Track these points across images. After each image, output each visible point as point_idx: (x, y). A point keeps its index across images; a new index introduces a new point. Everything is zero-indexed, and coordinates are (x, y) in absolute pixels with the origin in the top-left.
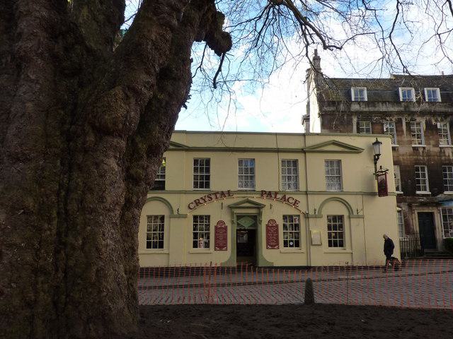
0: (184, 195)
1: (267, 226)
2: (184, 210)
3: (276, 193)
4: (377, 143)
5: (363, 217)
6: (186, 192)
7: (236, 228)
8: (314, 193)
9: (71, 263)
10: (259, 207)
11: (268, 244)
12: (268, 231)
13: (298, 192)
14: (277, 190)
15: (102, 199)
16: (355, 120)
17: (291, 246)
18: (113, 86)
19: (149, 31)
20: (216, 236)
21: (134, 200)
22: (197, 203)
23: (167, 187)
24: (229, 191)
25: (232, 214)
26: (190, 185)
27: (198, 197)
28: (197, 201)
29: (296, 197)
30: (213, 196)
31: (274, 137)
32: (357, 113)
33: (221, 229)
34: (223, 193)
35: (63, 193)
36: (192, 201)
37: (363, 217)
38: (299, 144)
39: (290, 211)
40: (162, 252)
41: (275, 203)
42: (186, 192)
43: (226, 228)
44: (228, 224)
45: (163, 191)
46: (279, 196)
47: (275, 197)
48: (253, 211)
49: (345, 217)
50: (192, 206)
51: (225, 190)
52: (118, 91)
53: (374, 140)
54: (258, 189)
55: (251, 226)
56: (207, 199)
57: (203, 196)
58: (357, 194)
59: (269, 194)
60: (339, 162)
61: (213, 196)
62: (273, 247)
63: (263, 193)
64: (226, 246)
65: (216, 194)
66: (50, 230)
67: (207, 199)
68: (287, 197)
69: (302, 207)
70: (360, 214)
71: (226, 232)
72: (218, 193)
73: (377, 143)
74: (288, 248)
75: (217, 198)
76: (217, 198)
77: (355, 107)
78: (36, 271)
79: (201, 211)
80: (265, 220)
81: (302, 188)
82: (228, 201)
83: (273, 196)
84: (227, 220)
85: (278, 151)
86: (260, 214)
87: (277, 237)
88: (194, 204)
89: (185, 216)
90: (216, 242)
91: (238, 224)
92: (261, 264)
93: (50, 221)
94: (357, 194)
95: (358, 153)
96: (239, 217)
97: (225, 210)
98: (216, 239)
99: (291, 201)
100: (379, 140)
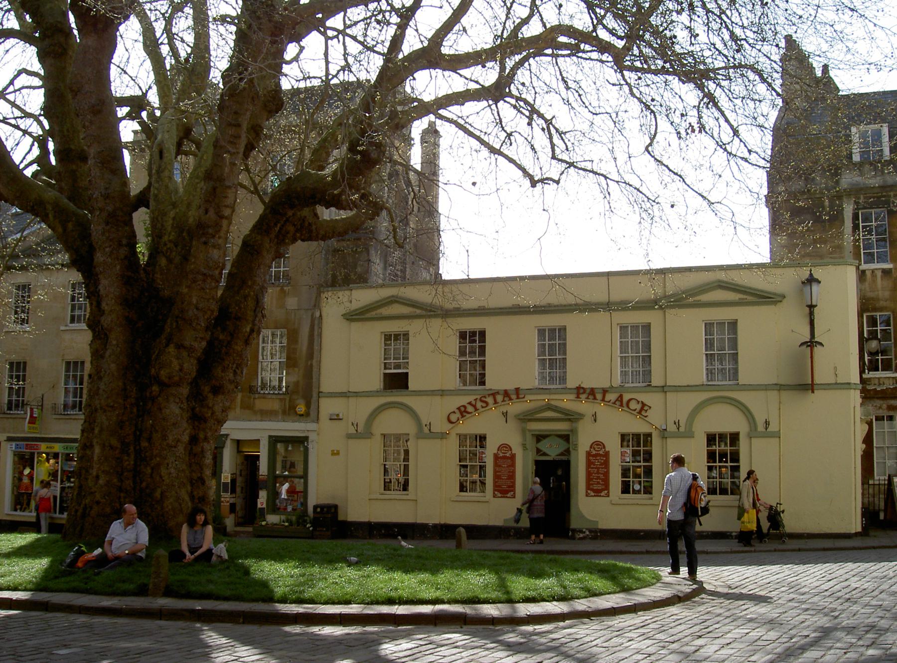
0: (437, 399)
1: (588, 454)
2: (440, 426)
3: (605, 391)
4: (811, 280)
5: (777, 435)
6: (442, 393)
7: (532, 456)
8: (678, 389)
9: (144, 485)
10: (572, 417)
11: (588, 487)
12: (589, 464)
13: (649, 387)
14: (606, 385)
15: (164, 437)
16: (848, 210)
17: (635, 492)
18: (167, 345)
19: (190, 297)
20: (495, 472)
21: (202, 435)
22: (463, 411)
23: (412, 385)
24: (517, 389)
25: (524, 431)
26: (452, 380)
27: (463, 400)
28: (463, 409)
29: (642, 397)
30: (490, 400)
31: (605, 279)
32: (855, 191)
33: (505, 459)
34: (506, 393)
35: (138, 433)
36: (454, 408)
37: (777, 435)
38: (649, 292)
39: (637, 426)
40: (405, 497)
41: (601, 409)
42: (442, 393)
43: (513, 457)
44: (517, 450)
45: (404, 392)
46: (611, 397)
47: (603, 400)
48: (562, 427)
49: (741, 437)
50: (453, 418)
51: (510, 387)
52: (171, 349)
53: (805, 273)
54: (572, 383)
55: (562, 454)
56: (479, 404)
57: (471, 398)
58: (766, 388)
59: (592, 392)
60: (733, 325)
61: (490, 400)
62: (597, 493)
63: (579, 391)
64: (514, 491)
65: (494, 394)
66: (129, 462)
67: (479, 404)
68: (626, 397)
69: (655, 417)
70: (773, 428)
71: (513, 465)
72: (498, 393)
73: (811, 280)
74: (631, 496)
75: (496, 402)
76: (496, 402)
77: (848, 179)
78: (120, 489)
79: (472, 426)
80: (583, 444)
81: (656, 380)
82: (515, 408)
83: (599, 396)
84: (515, 442)
85: (608, 306)
86: (574, 431)
87: (607, 474)
88: (458, 415)
89: (443, 436)
90: (495, 482)
91: (538, 451)
92: (574, 524)
93: (128, 455)
94: (766, 388)
95: (775, 303)
96: (540, 437)
97: (513, 424)
98: (497, 477)
99: (633, 405)
100: (818, 273)
